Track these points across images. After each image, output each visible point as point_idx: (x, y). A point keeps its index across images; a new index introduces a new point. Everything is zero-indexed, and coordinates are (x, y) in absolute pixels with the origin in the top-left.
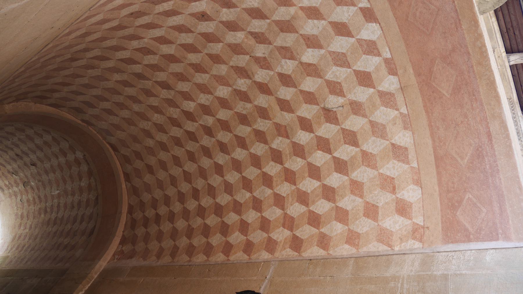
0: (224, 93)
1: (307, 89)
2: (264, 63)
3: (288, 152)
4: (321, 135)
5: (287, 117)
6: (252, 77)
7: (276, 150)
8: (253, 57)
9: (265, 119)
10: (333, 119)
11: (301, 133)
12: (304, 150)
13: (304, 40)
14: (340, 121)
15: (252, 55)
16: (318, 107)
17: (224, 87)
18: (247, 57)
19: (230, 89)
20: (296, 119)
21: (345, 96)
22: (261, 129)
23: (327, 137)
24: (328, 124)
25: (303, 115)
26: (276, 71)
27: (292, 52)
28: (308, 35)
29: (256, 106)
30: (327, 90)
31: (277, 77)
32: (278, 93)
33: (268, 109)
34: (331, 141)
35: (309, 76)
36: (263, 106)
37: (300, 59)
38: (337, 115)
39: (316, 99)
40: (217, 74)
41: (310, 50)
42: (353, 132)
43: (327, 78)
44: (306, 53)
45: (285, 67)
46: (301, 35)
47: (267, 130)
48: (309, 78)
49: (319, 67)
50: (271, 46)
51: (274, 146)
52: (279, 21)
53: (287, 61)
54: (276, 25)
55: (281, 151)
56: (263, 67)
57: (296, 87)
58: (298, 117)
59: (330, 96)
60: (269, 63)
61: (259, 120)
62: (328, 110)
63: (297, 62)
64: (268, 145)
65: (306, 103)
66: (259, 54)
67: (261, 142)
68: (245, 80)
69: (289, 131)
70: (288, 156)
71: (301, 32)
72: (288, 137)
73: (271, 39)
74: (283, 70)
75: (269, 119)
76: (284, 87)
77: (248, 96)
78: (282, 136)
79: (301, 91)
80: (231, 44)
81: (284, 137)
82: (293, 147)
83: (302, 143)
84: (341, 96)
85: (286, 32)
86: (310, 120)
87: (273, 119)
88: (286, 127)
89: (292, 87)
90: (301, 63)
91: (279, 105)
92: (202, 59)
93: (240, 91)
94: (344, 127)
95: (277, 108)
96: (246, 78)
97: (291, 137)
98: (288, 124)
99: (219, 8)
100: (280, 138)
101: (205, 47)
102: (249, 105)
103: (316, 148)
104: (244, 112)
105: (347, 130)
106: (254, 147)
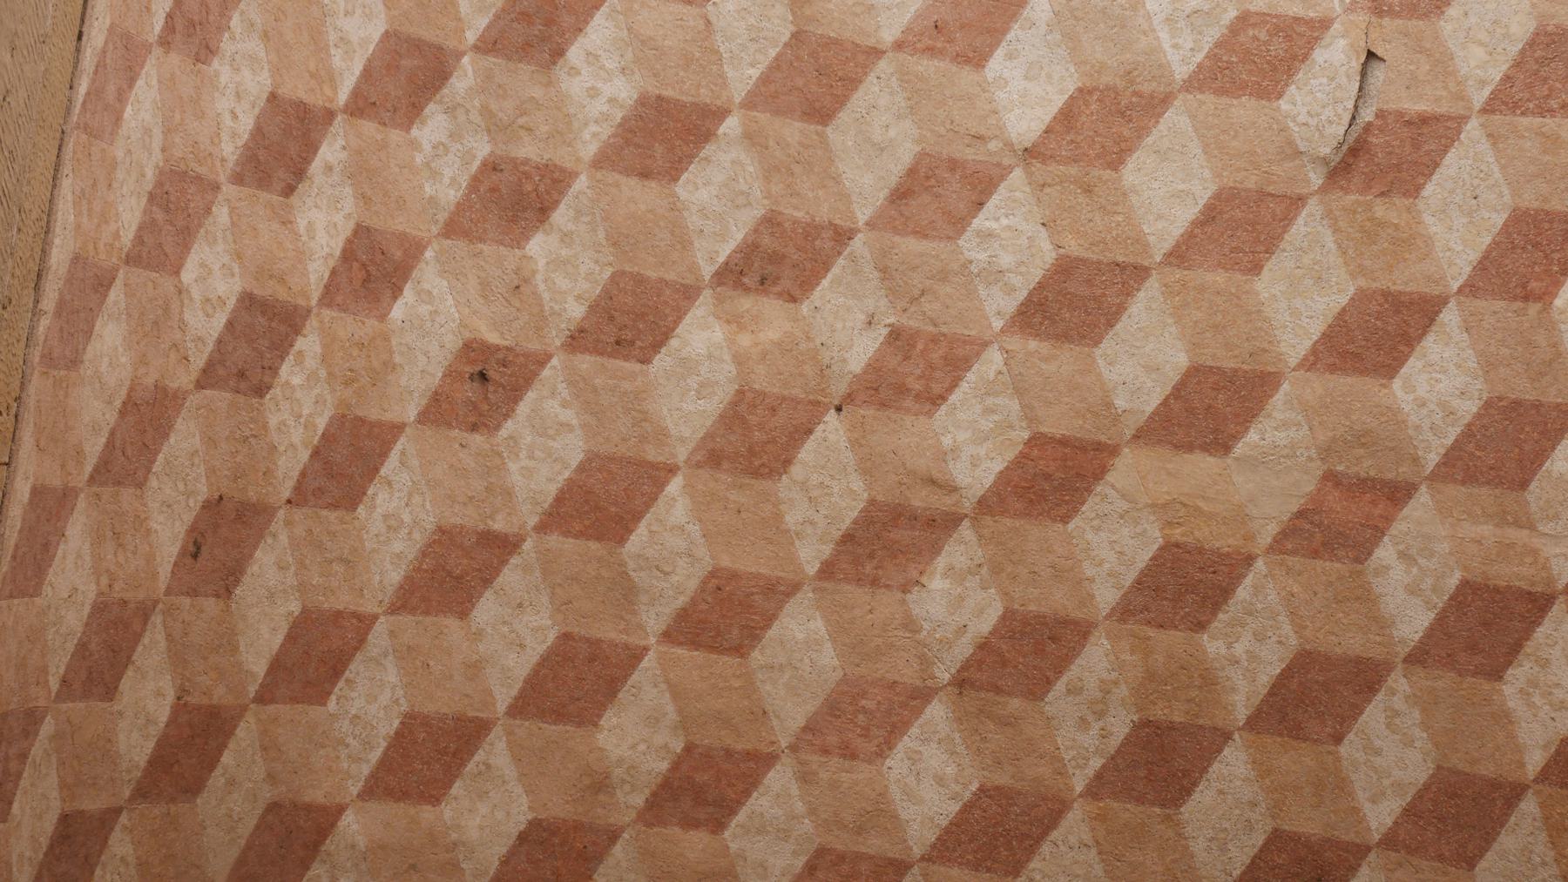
0: (940, 780)
1: (1183, 216)
2: (919, 369)
3: (1486, 530)
4: (1474, 256)
5: (1281, 437)
6: (945, 502)
7: (1441, 619)
8: (850, 398)
9: (1226, 592)
10: (1417, 146)
11: (1409, 388)
12: (1517, 403)
13: (930, 51)
14: (1443, 109)
15: (839, 389)
16: (1313, 207)
17: (907, 743)
18: (832, 427)
19: (937, 712)
20: (1318, 385)
21: (1325, 24)
22: (1272, 665)
23: (1499, 220)
24: (1429, 189)
25: (1316, 329)
26: (998, 324)
27: (954, 165)
28: (918, 16)
29: (1124, 612)
30: (1244, 109)
31: (1033, 344)
32: (1120, 403)
33: (1177, 534)
34: (1529, 200)
35: (1122, 161)
36: (1144, 557)
37: (1009, 145)
38: (1400, 114)
39: (1262, 195)
40: (811, 707)
41: (997, 64)
42: (1531, 44)
43: (1181, 72)
44: (1001, 95)
45: (1006, 260)
46: (899, 46)
47: (1299, 629)
48: (1131, 164)
49: (1106, 79)
50: (858, 243)
51: (1413, 622)
52: (765, 79)
53: (981, 222)
54: (777, 112)
55: (1465, 583)
56: (937, 388)
57: (1140, 273)
58: (1312, 362)
59: (1284, 104)
60: (934, 340)
61: (1212, 645)
62: (1354, 151)
63: (1017, 175)
64: (1388, 667)
65: (1256, 268)
66: (858, 351)
67: (1357, 710)
68: (941, 562)
69: (1367, 467)
70: (1513, 534)
71: (888, 36)
72: (1398, 493)
73: (823, 214)
74: (1016, 280)
75: (1236, 565)
76: (1107, 345)
77: (1041, 619)
78: (1379, 532)
79: (1179, 255)
80: (709, 436)
81: (1388, 520)
82: (1470, 478)
83: (1469, 408)
84: (1312, 43)
85: (841, 101)
86: (1361, 297)
87: (1250, 537)
88: (1331, 477)
89: (1128, 293)
90: (1031, 154)
91: (1190, 448)
92: (676, 693)
93: (984, 646)
94: (1486, 92)
95: (1202, 465)
96: (936, 550)
97: (1404, 471)
98: (1326, 452)
99: (511, 257)
100: (1385, 553)
101: (625, 593)
102: (1096, 661)
103: (1534, 309)
104: (1120, 725)
105: (1507, 78)
106: (1360, 782)
